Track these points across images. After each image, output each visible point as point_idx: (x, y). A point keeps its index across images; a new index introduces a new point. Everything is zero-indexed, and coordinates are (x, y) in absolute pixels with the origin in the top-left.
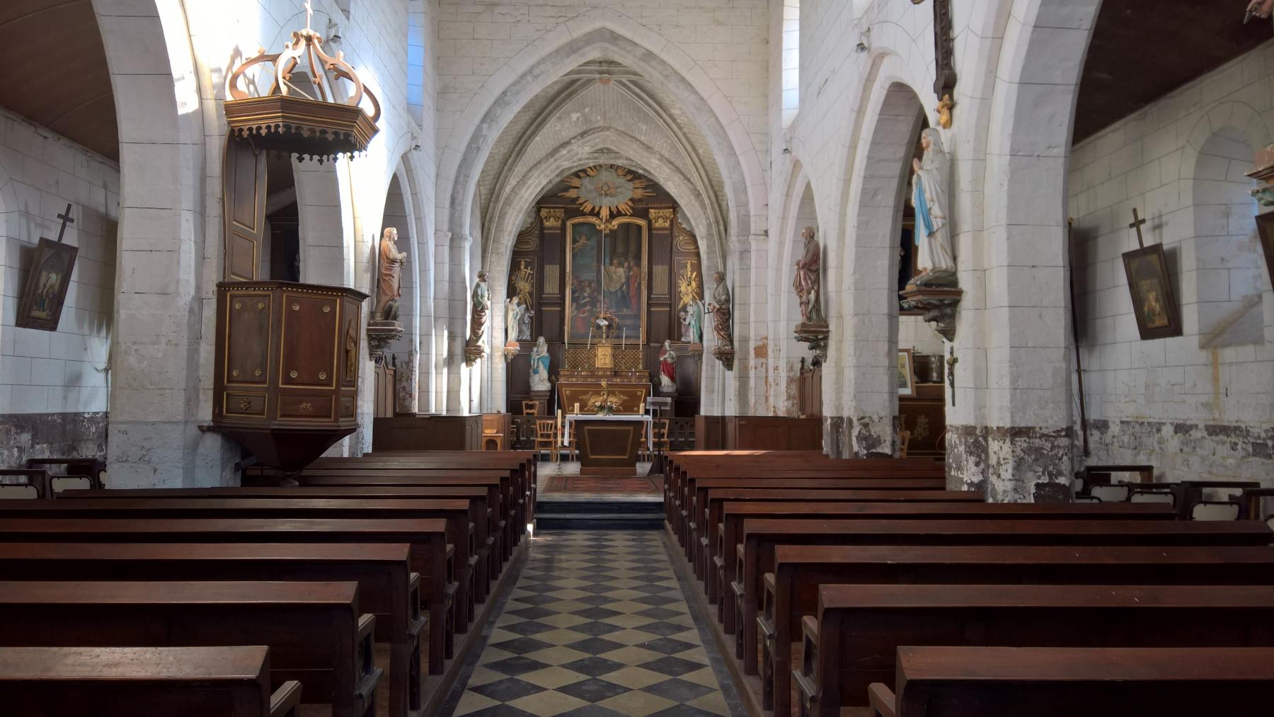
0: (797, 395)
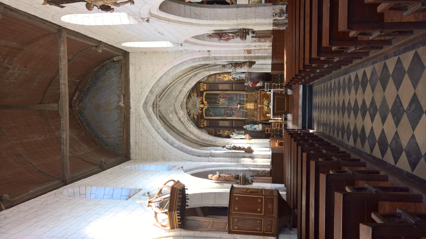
0: (265, 39)
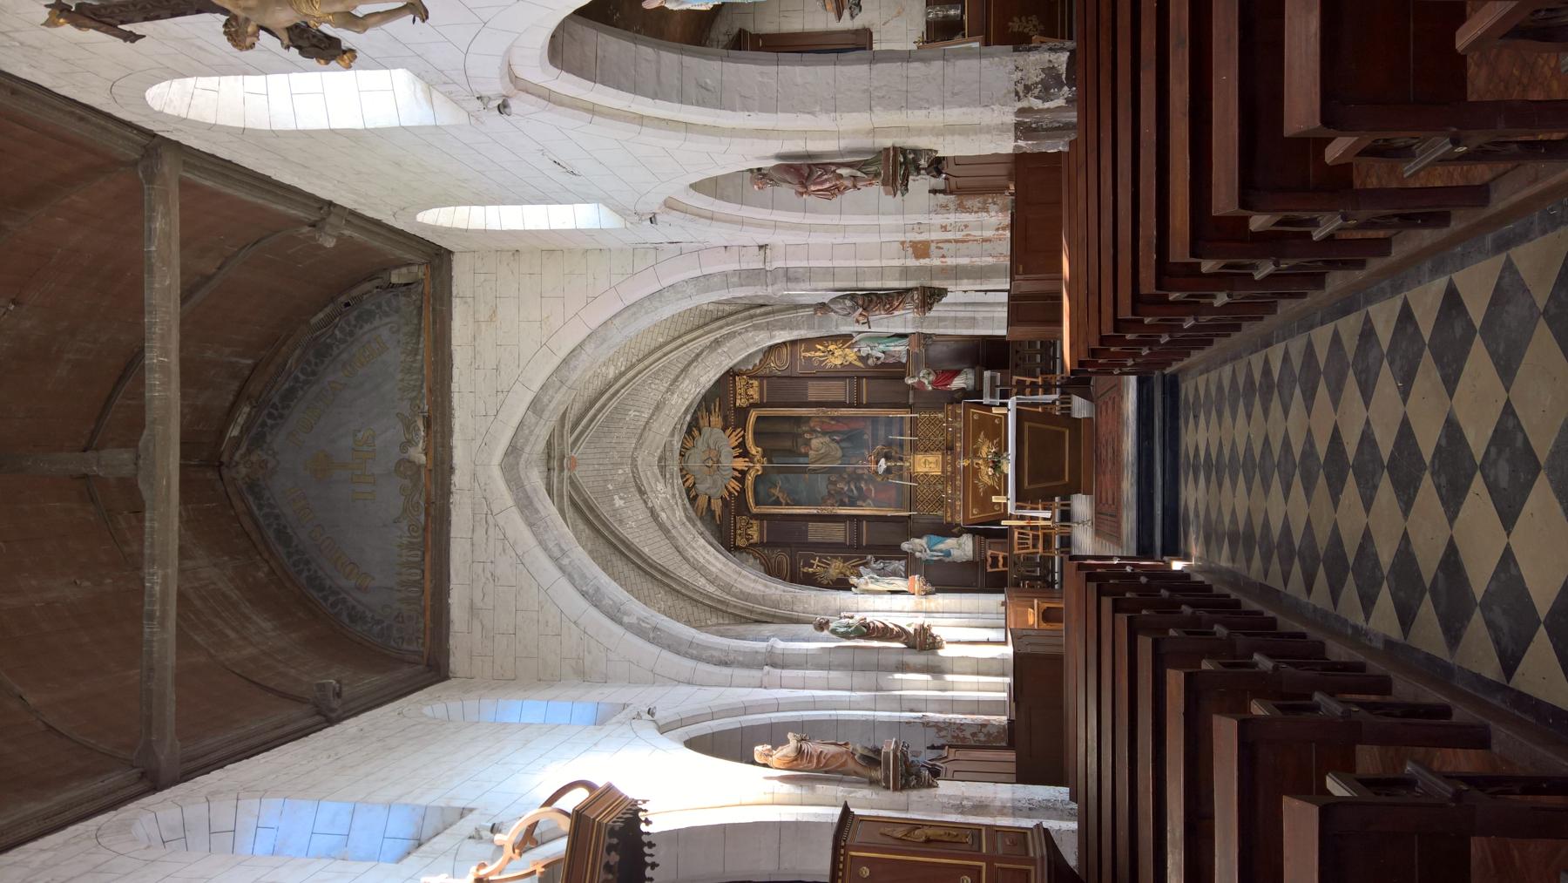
0: (981, 199)
